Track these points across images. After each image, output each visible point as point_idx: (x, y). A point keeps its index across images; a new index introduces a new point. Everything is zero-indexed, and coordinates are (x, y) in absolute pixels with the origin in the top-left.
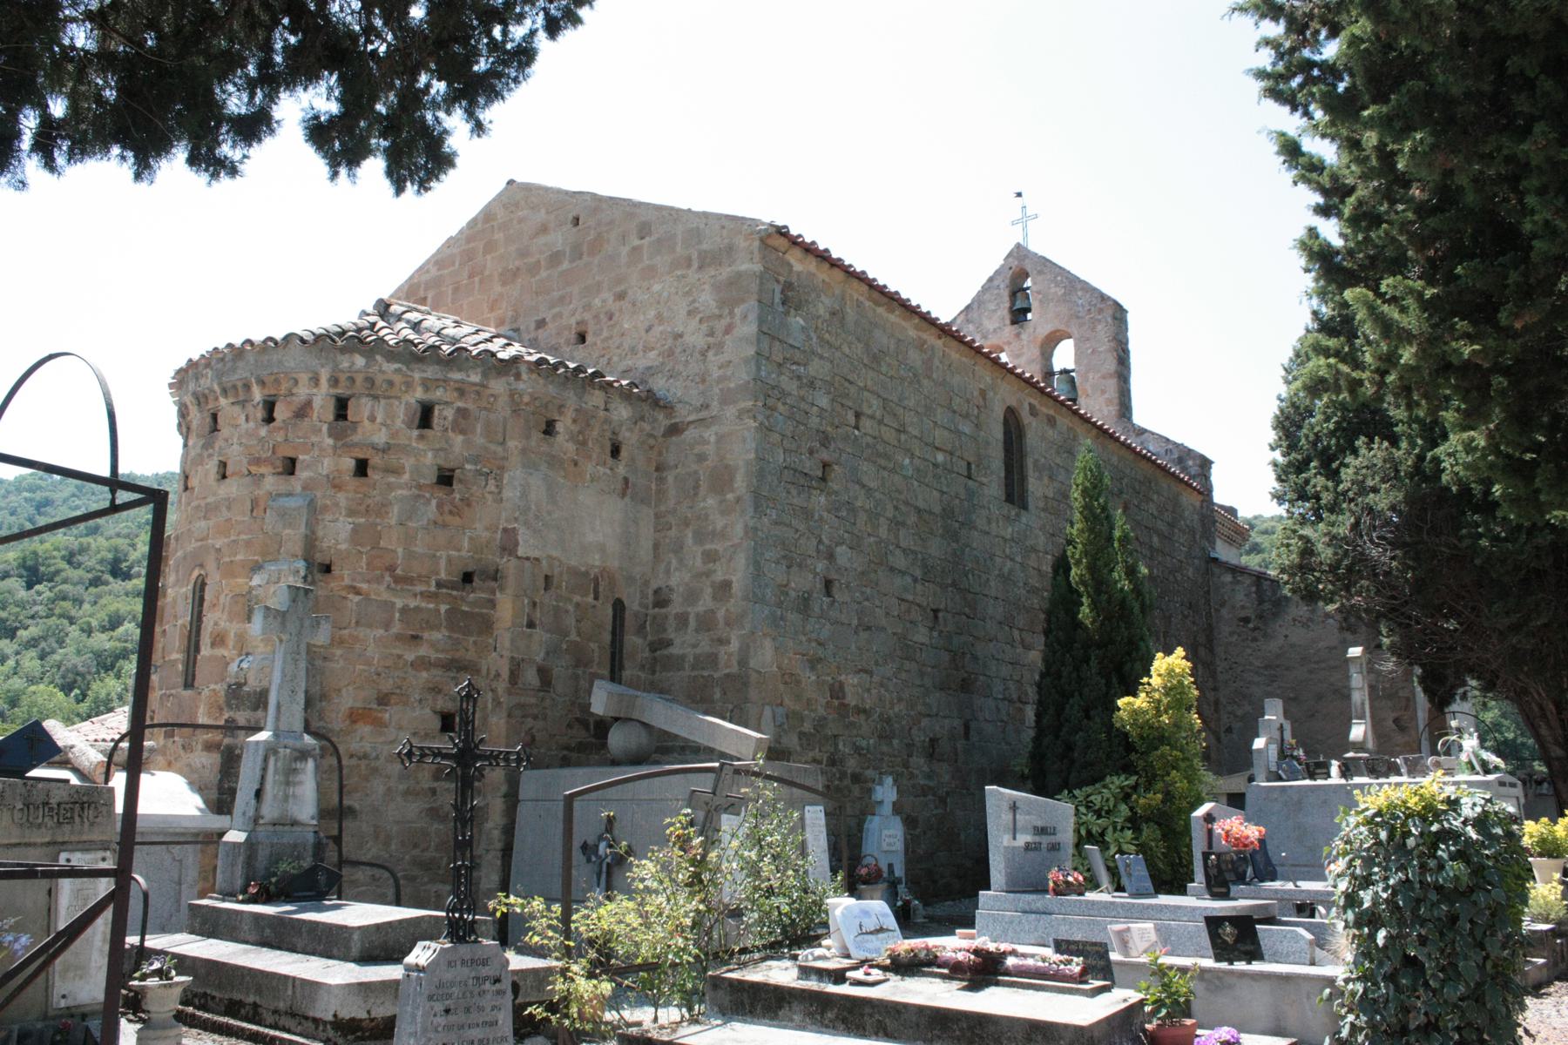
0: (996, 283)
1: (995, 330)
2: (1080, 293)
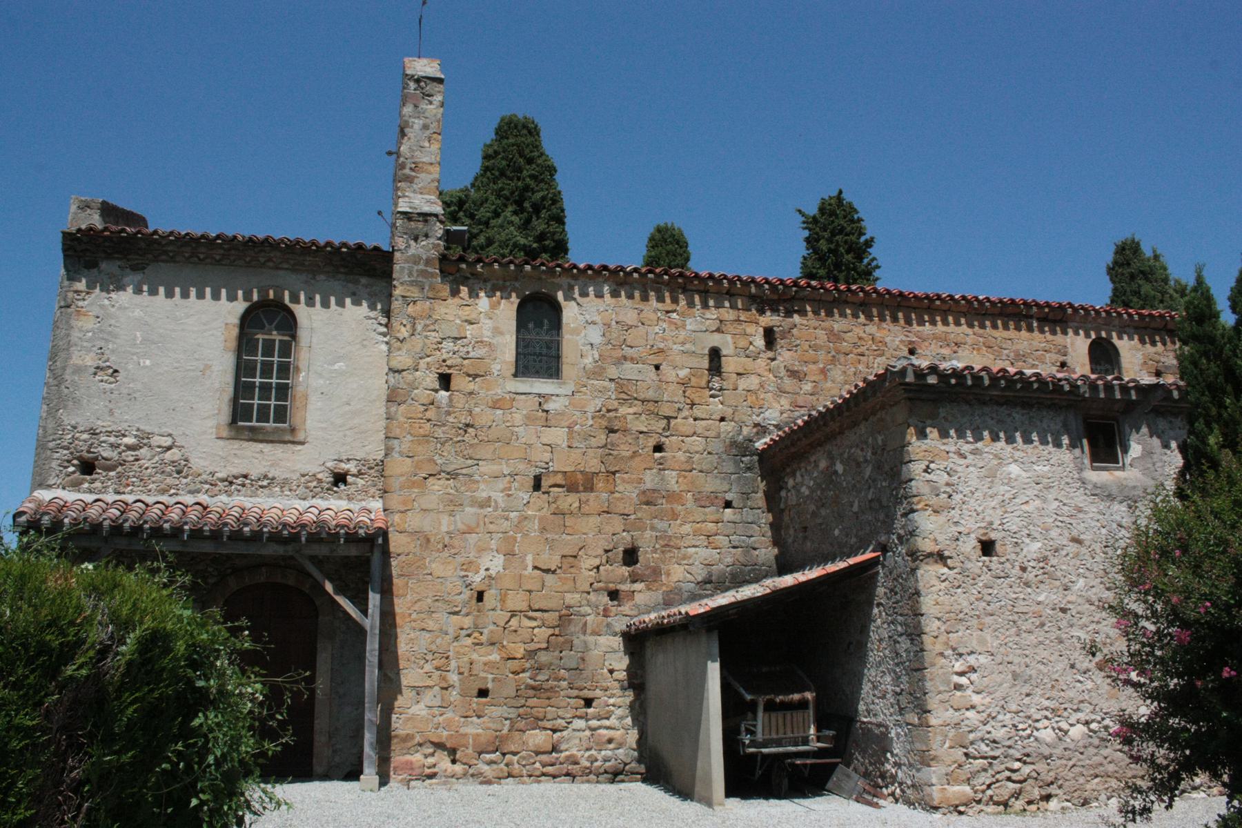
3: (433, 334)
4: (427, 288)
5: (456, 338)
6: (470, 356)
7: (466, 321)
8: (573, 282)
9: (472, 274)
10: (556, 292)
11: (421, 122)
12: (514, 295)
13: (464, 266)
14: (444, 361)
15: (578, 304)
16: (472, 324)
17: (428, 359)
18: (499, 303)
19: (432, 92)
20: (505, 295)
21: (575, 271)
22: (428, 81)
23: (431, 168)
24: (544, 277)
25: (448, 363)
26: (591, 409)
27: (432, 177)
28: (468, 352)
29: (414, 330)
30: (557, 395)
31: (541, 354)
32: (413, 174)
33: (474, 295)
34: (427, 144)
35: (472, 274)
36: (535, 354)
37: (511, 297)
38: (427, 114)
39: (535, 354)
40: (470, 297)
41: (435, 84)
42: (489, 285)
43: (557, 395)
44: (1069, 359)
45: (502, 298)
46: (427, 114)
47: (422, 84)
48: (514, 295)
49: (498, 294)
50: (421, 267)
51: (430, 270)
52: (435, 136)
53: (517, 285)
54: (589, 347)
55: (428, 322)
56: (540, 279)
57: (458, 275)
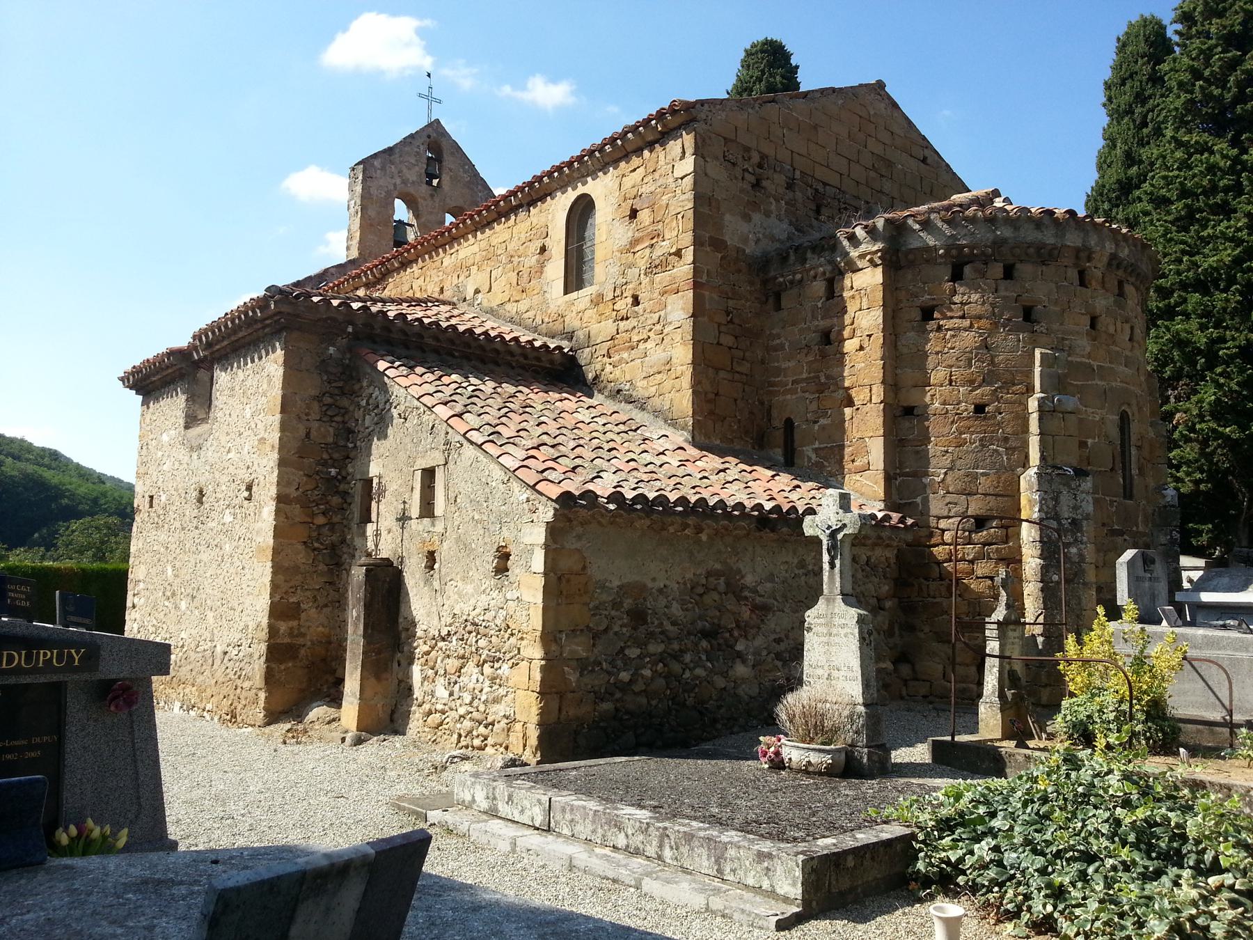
0: (418, 142)
1: (413, 182)
2: (480, 187)
44: (548, 242)
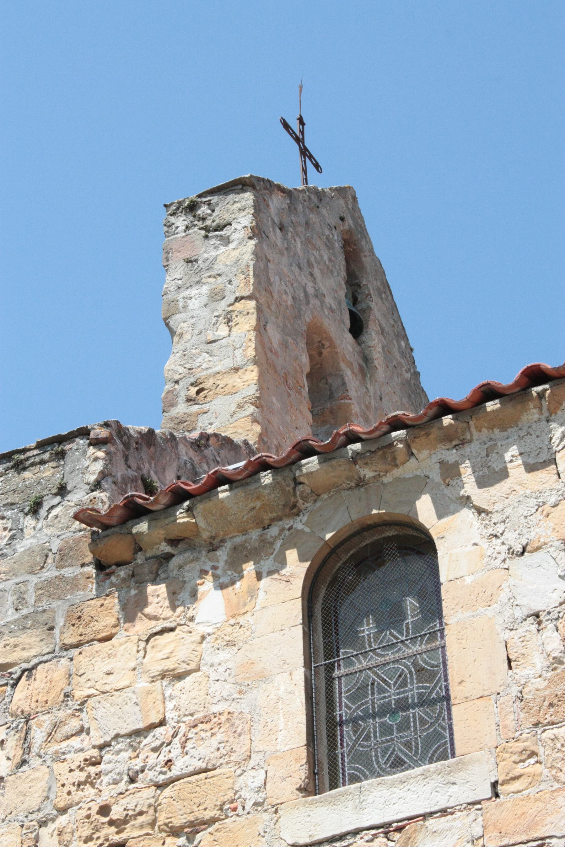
3: (75, 742)
4: (60, 622)
5: (137, 733)
6: (175, 771)
7: (163, 676)
8: (452, 456)
9: (173, 542)
10: (412, 504)
11: (205, 289)
12: (292, 555)
13: (143, 527)
14: (104, 810)
15: (480, 511)
16: (180, 677)
17: (63, 820)
18: (252, 593)
19: (227, 217)
20: (268, 563)
21: (447, 420)
22: (214, 199)
23: (235, 380)
24: (368, 473)
25: (116, 813)
26: (85, 713)
27: (238, 398)
28: (169, 763)
29: (27, 750)
30: (444, 812)
31: (403, 705)
32: (195, 408)
33: (185, 595)
34: (223, 330)
35: (173, 542)
36: (385, 710)
37: (283, 562)
38: (218, 267)
39: (385, 710)
40: (174, 607)
41: (231, 197)
42: (222, 555)
43: (444, 812)
45: (259, 577)
46: (218, 267)
47: (204, 210)
48: (292, 555)
49: (249, 568)
50: (50, 573)
51: (68, 572)
52: (239, 306)
53: (299, 524)
54: (530, 625)
55: (61, 714)
56: (361, 483)
57: (140, 558)
